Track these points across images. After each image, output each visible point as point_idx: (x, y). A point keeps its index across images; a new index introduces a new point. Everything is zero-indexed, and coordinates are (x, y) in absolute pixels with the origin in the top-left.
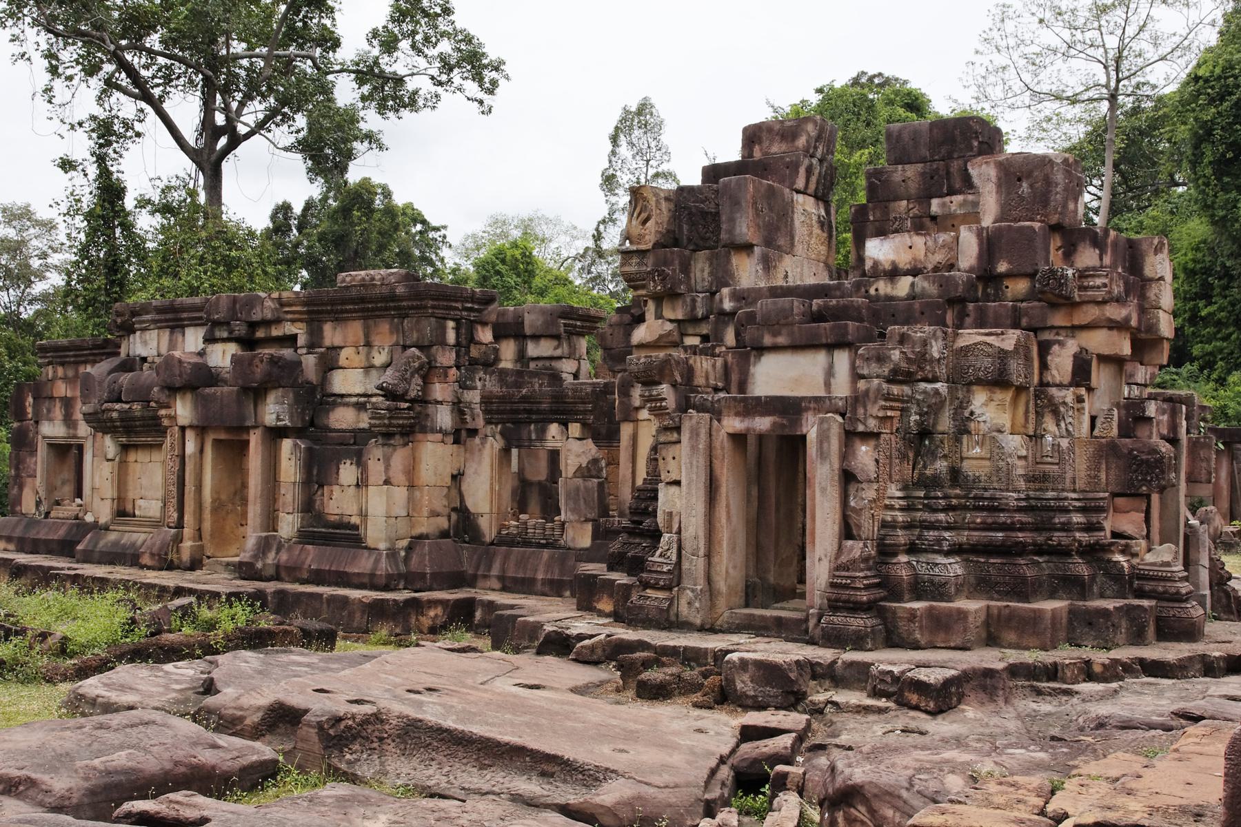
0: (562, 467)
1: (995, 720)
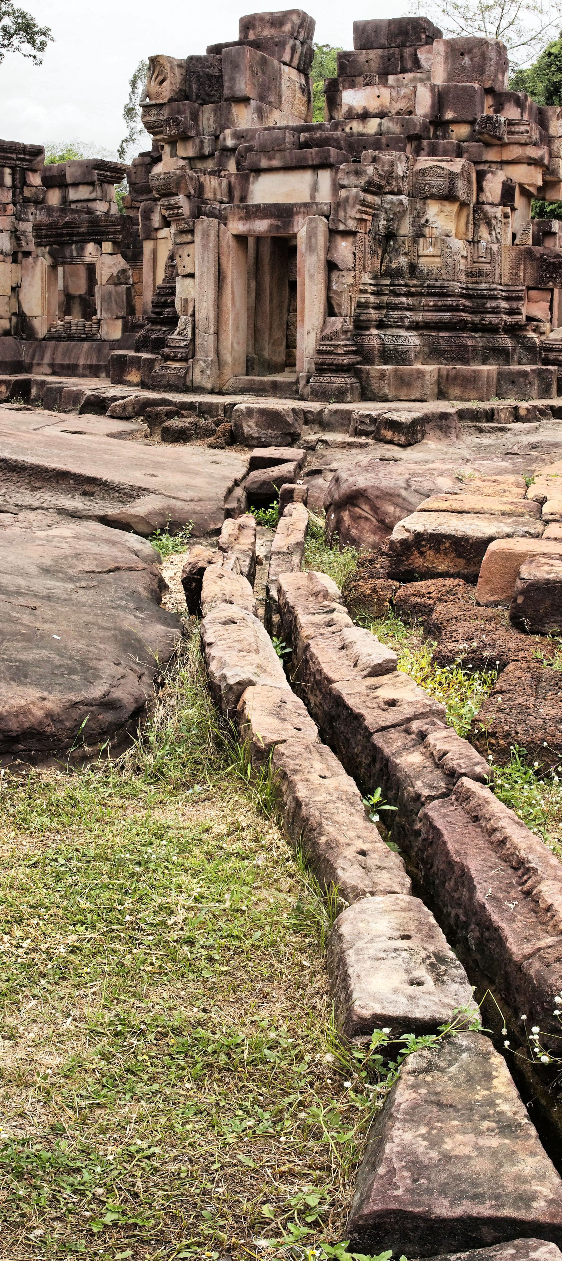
0: (98, 276)
1: (451, 450)
